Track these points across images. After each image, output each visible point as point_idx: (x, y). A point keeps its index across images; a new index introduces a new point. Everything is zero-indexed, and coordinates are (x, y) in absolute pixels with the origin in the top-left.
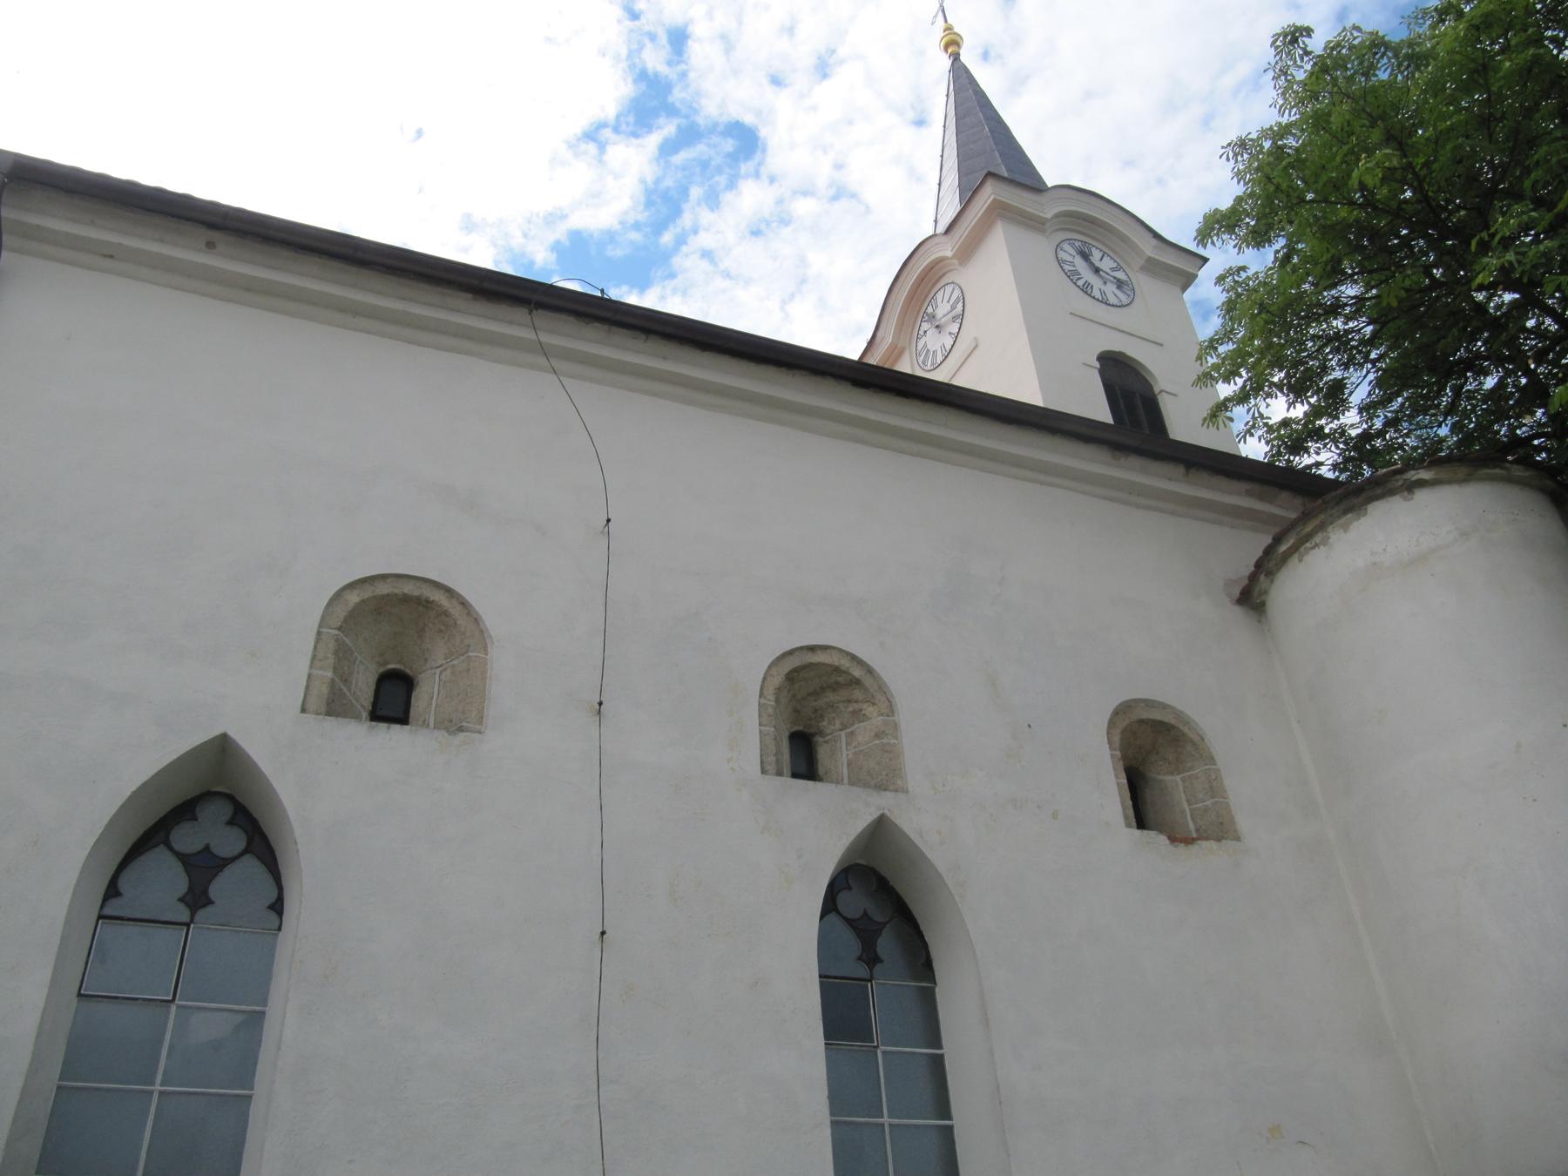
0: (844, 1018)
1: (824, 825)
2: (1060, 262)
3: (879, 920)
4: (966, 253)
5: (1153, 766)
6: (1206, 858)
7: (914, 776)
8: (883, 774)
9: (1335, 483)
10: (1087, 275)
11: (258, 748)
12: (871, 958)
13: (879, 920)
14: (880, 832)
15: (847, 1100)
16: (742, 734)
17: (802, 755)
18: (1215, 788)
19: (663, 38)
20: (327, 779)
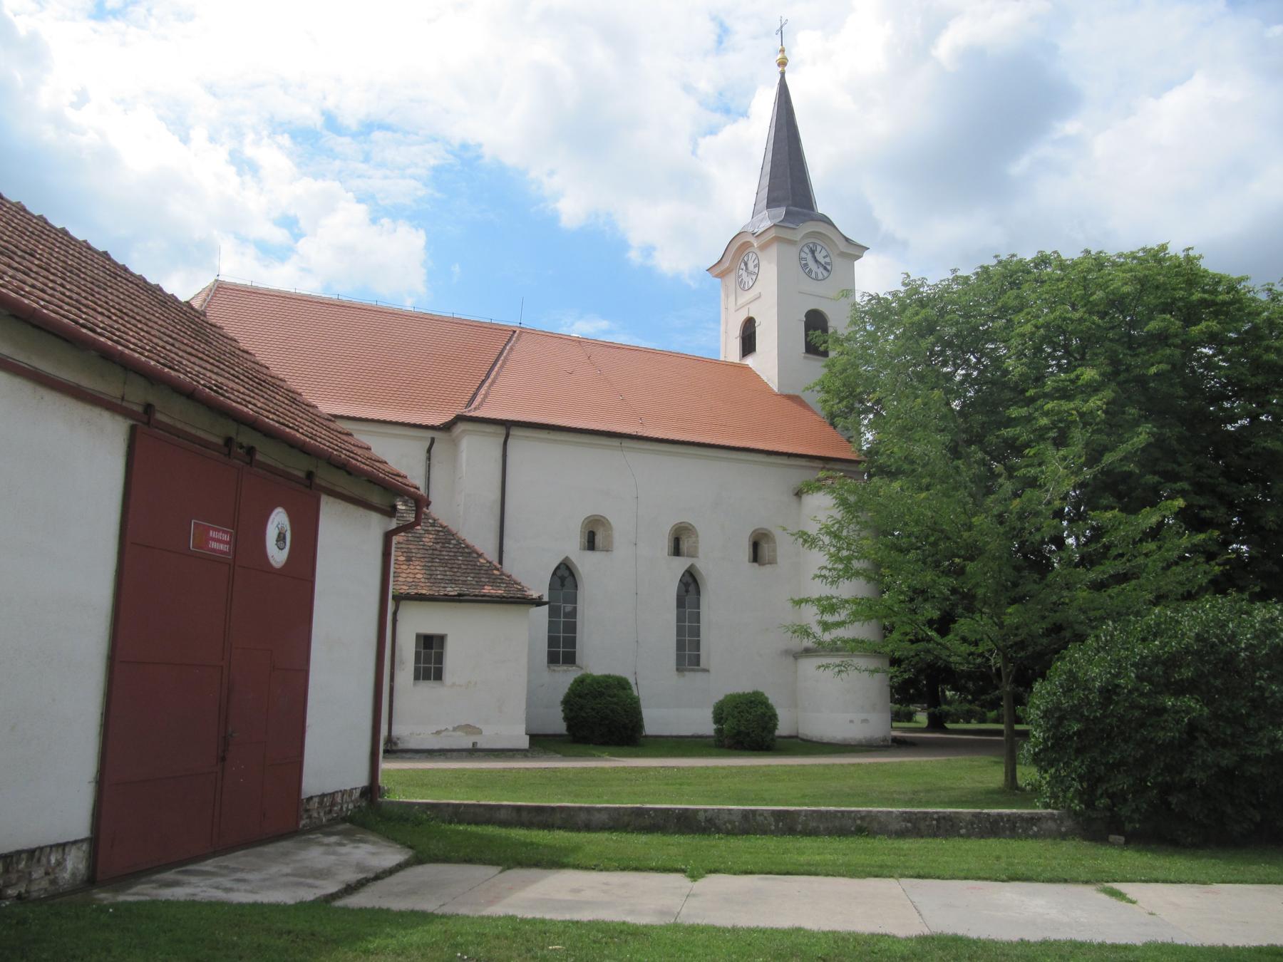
0: (681, 603)
1: (681, 565)
2: (801, 259)
3: (690, 585)
4: (763, 247)
5: (758, 549)
6: (767, 569)
7: (701, 554)
8: (693, 555)
9: (1023, 790)
10: (812, 265)
11: (574, 558)
12: (687, 591)
13: (690, 585)
14: (692, 566)
15: (680, 619)
16: (665, 544)
17: (677, 551)
18: (774, 551)
19: (717, 118)
20: (586, 564)
